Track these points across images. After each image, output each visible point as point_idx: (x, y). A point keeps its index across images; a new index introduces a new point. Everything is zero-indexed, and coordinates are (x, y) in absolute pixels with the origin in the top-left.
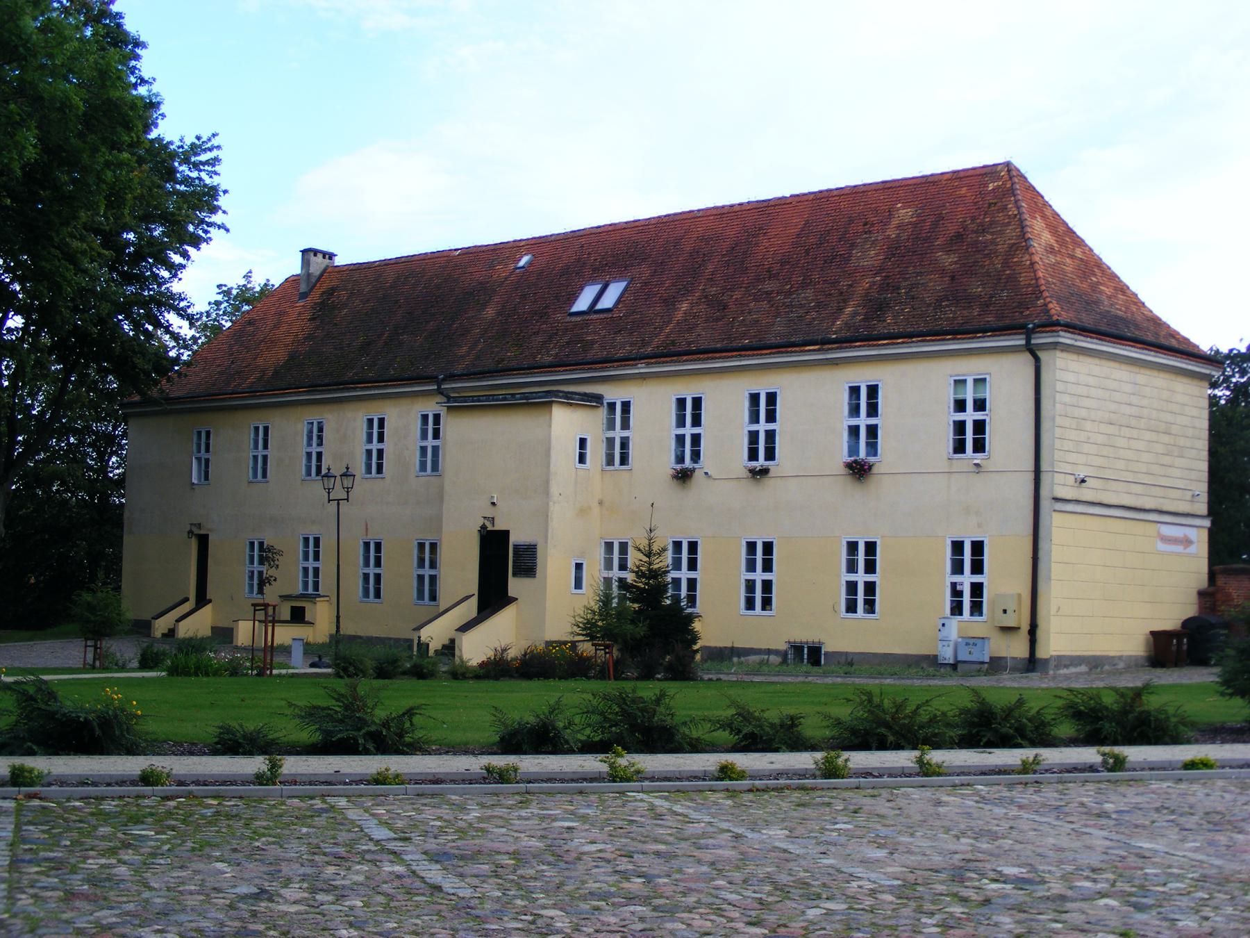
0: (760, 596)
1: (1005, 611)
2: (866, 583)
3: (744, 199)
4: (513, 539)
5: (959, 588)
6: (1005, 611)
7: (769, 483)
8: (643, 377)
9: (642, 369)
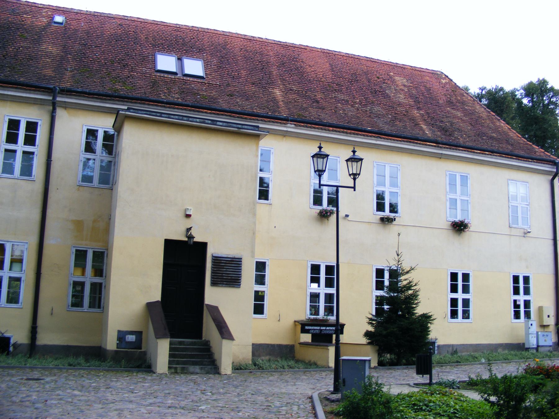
0: (458, 309)
1: (549, 316)
2: (463, 300)
3: (190, 23)
4: (211, 251)
5: (518, 303)
6: (549, 316)
7: (393, 228)
8: (285, 134)
9: (290, 128)
